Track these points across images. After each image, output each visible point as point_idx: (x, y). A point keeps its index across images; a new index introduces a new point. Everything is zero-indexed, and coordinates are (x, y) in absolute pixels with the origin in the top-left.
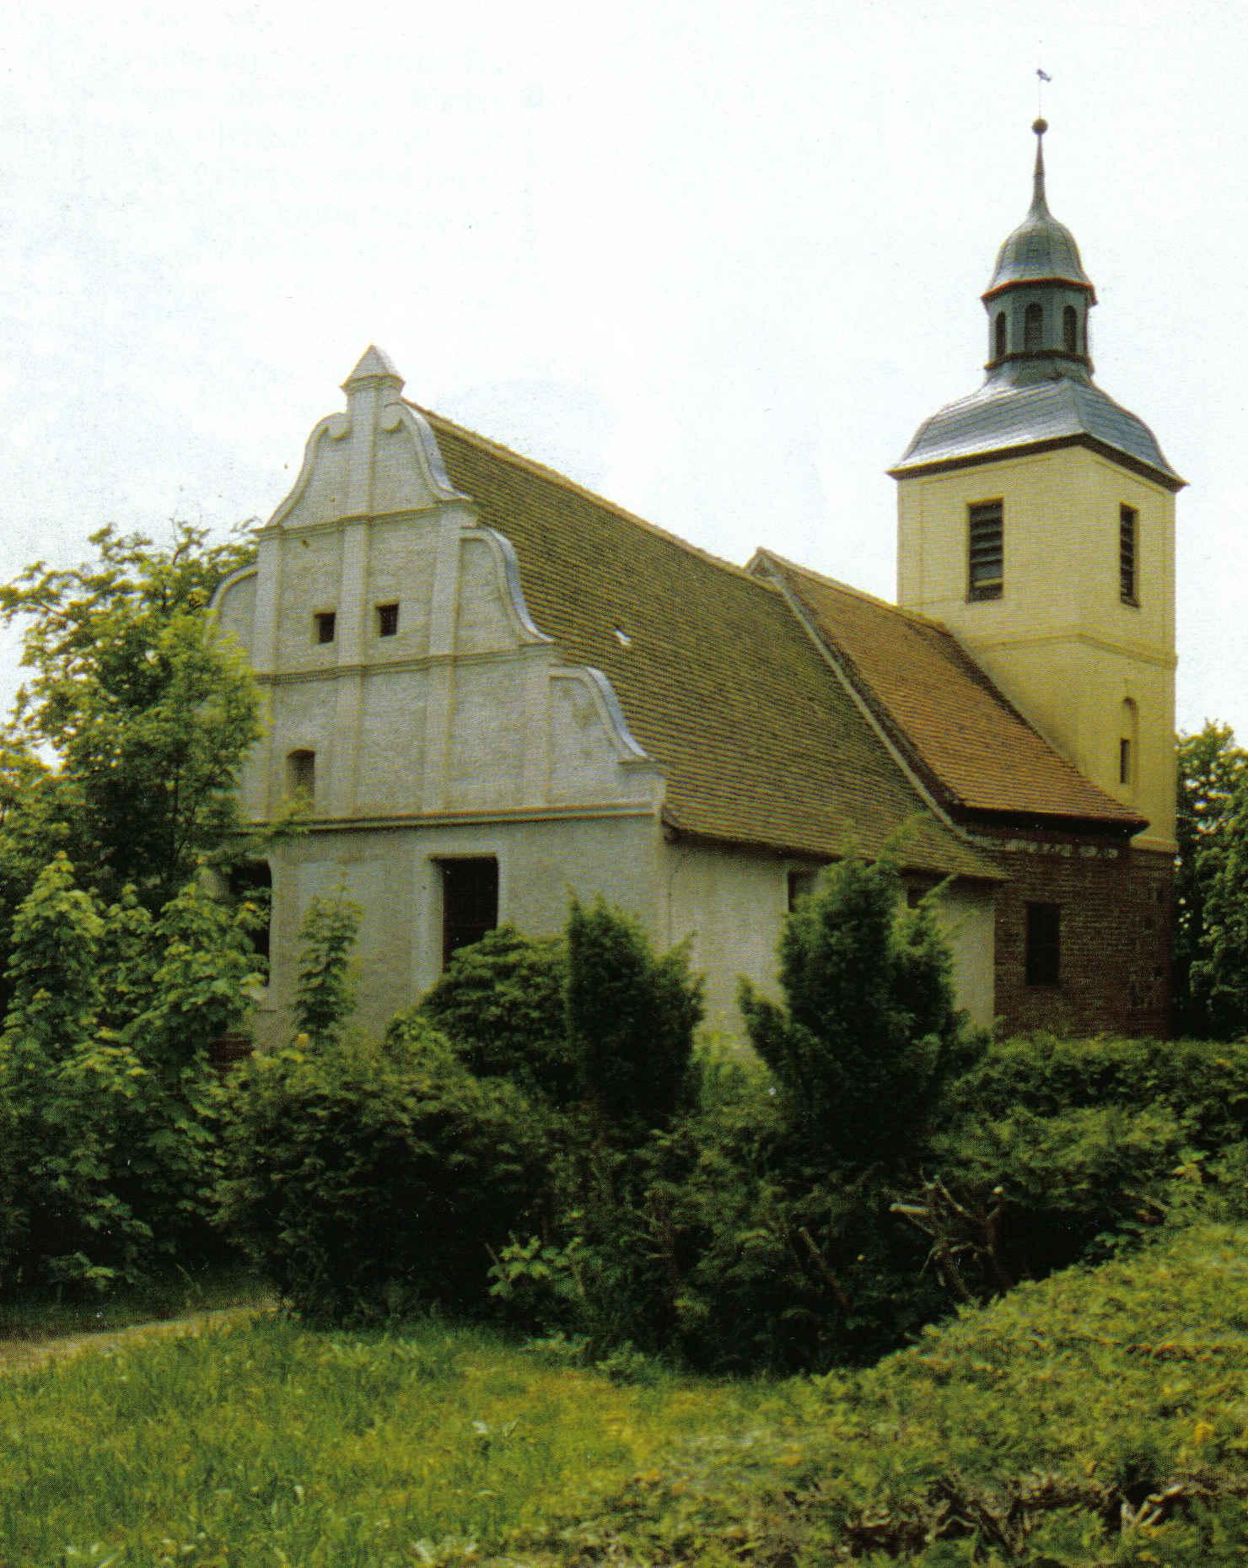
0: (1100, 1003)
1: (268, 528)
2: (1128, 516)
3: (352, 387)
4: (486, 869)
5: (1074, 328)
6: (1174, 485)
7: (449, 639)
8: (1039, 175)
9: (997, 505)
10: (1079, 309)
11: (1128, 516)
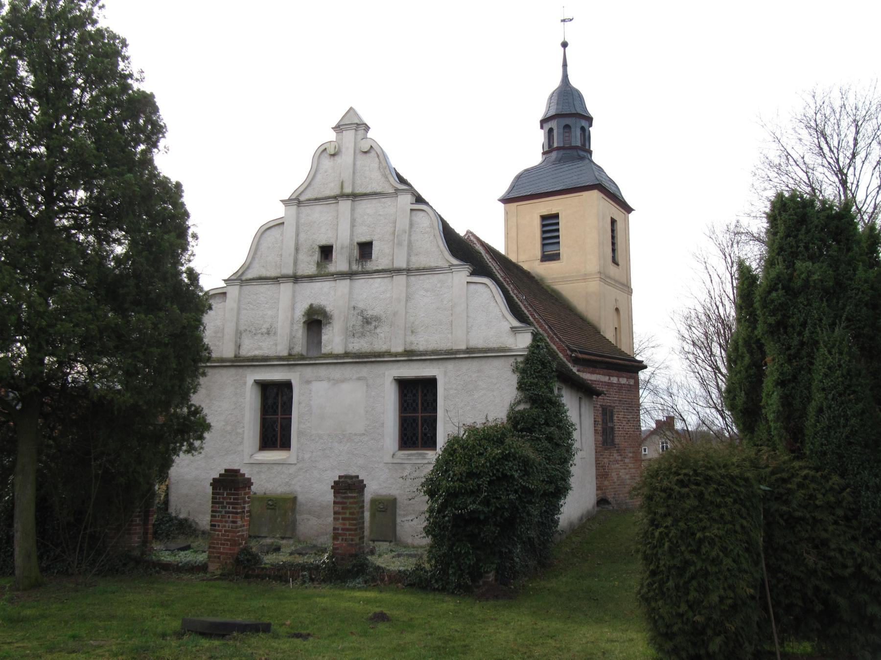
0: (631, 455)
1: (290, 200)
2: (613, 222)
3: (338, 128)
4: (430, 384)
5: (584, 135)
6: (628, 209)
7: (405, 259)
8: (565, 65)
9: (556, 216)
10: (586, 128)
11: (613, 222)
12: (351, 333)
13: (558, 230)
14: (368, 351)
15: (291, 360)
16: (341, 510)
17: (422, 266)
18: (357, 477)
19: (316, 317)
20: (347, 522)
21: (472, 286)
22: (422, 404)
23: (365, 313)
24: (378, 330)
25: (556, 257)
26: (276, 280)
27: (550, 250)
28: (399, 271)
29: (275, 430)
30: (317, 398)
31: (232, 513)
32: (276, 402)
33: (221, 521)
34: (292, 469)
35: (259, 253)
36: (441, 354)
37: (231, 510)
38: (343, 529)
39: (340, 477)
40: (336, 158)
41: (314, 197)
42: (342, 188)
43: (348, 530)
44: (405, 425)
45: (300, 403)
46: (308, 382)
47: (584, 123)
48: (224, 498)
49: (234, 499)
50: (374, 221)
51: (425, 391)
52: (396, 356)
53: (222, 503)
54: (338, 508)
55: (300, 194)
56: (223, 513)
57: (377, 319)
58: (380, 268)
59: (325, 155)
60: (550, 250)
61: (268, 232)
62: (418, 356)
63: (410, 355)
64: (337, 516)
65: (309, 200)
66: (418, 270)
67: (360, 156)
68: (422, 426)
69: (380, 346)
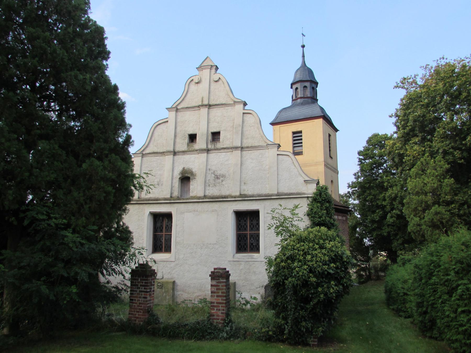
1: (171, 108)
2: (330, 135)
6: (336, 130)
8: (303, 56)
9: (301, 132)
12: (206, 184)
13: (301, 139)
14: (218, 194)
15: (171, 200)
16: (215, 291)
17: (250, 145)
18: (225, 269)
19: (186, 175)
20: (220, 298)
21: (280, 156)
22: (250, 226)
23: (216, 172)
24: (224, 183)
25: (300, 153)
26: (163, 153)
27: (297, 150)
28: (236, 148)
29: (161, 243)
30: (185, 222)
31: (144, 292)
32: (162, 223)
33: (136, 297)
34: (173, 264)
35: (153, 138)
36: (263, 196)
37: (143, 290)
38: (217, 303)
39: (215, 269)
40: (199, 85)
41: (186, 106)
42: (202, 101)
43: (220, 303)
44: (240, 239)
45: (176, 225)
46: (182, 213)
47: (314, 85)
48: (138, 282)
49: (145, 283)
50: (220, 120)
51: (252, 219)
52: (235, 197)
53: (138, 285)
54: (214, 289)
55: (178, 105)
56: (138, 292)
57: (223, 176)
58: (225, 146)
59: (193, 84)
60: (297, 150)
61: (159, 126)
62: (248, 197)
63: (244, 198)
64: (213, 294)
65: (183, 108)
66: (248, 147)
67: (213, 84)
68: (250, 239)
69: (225, 192)
